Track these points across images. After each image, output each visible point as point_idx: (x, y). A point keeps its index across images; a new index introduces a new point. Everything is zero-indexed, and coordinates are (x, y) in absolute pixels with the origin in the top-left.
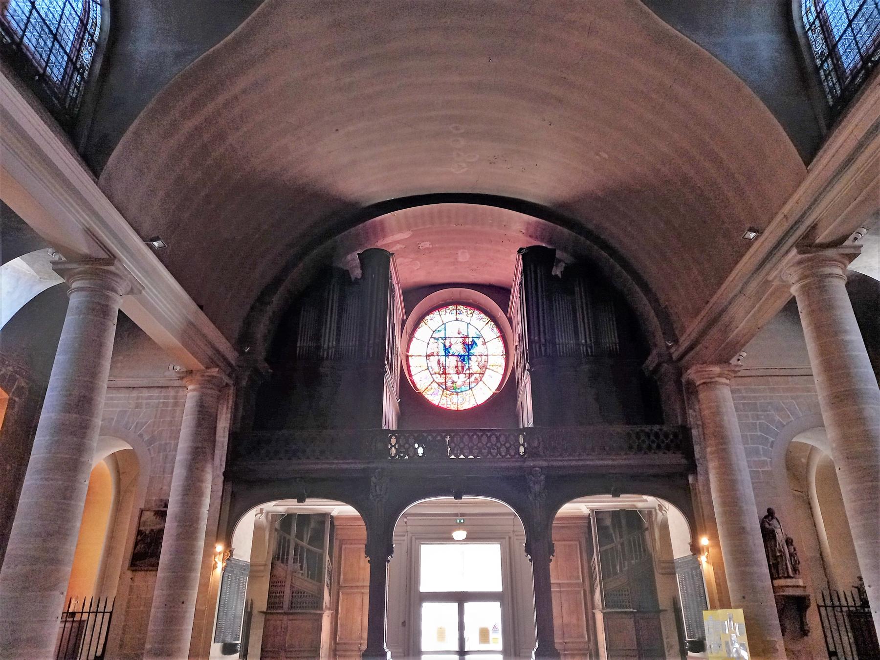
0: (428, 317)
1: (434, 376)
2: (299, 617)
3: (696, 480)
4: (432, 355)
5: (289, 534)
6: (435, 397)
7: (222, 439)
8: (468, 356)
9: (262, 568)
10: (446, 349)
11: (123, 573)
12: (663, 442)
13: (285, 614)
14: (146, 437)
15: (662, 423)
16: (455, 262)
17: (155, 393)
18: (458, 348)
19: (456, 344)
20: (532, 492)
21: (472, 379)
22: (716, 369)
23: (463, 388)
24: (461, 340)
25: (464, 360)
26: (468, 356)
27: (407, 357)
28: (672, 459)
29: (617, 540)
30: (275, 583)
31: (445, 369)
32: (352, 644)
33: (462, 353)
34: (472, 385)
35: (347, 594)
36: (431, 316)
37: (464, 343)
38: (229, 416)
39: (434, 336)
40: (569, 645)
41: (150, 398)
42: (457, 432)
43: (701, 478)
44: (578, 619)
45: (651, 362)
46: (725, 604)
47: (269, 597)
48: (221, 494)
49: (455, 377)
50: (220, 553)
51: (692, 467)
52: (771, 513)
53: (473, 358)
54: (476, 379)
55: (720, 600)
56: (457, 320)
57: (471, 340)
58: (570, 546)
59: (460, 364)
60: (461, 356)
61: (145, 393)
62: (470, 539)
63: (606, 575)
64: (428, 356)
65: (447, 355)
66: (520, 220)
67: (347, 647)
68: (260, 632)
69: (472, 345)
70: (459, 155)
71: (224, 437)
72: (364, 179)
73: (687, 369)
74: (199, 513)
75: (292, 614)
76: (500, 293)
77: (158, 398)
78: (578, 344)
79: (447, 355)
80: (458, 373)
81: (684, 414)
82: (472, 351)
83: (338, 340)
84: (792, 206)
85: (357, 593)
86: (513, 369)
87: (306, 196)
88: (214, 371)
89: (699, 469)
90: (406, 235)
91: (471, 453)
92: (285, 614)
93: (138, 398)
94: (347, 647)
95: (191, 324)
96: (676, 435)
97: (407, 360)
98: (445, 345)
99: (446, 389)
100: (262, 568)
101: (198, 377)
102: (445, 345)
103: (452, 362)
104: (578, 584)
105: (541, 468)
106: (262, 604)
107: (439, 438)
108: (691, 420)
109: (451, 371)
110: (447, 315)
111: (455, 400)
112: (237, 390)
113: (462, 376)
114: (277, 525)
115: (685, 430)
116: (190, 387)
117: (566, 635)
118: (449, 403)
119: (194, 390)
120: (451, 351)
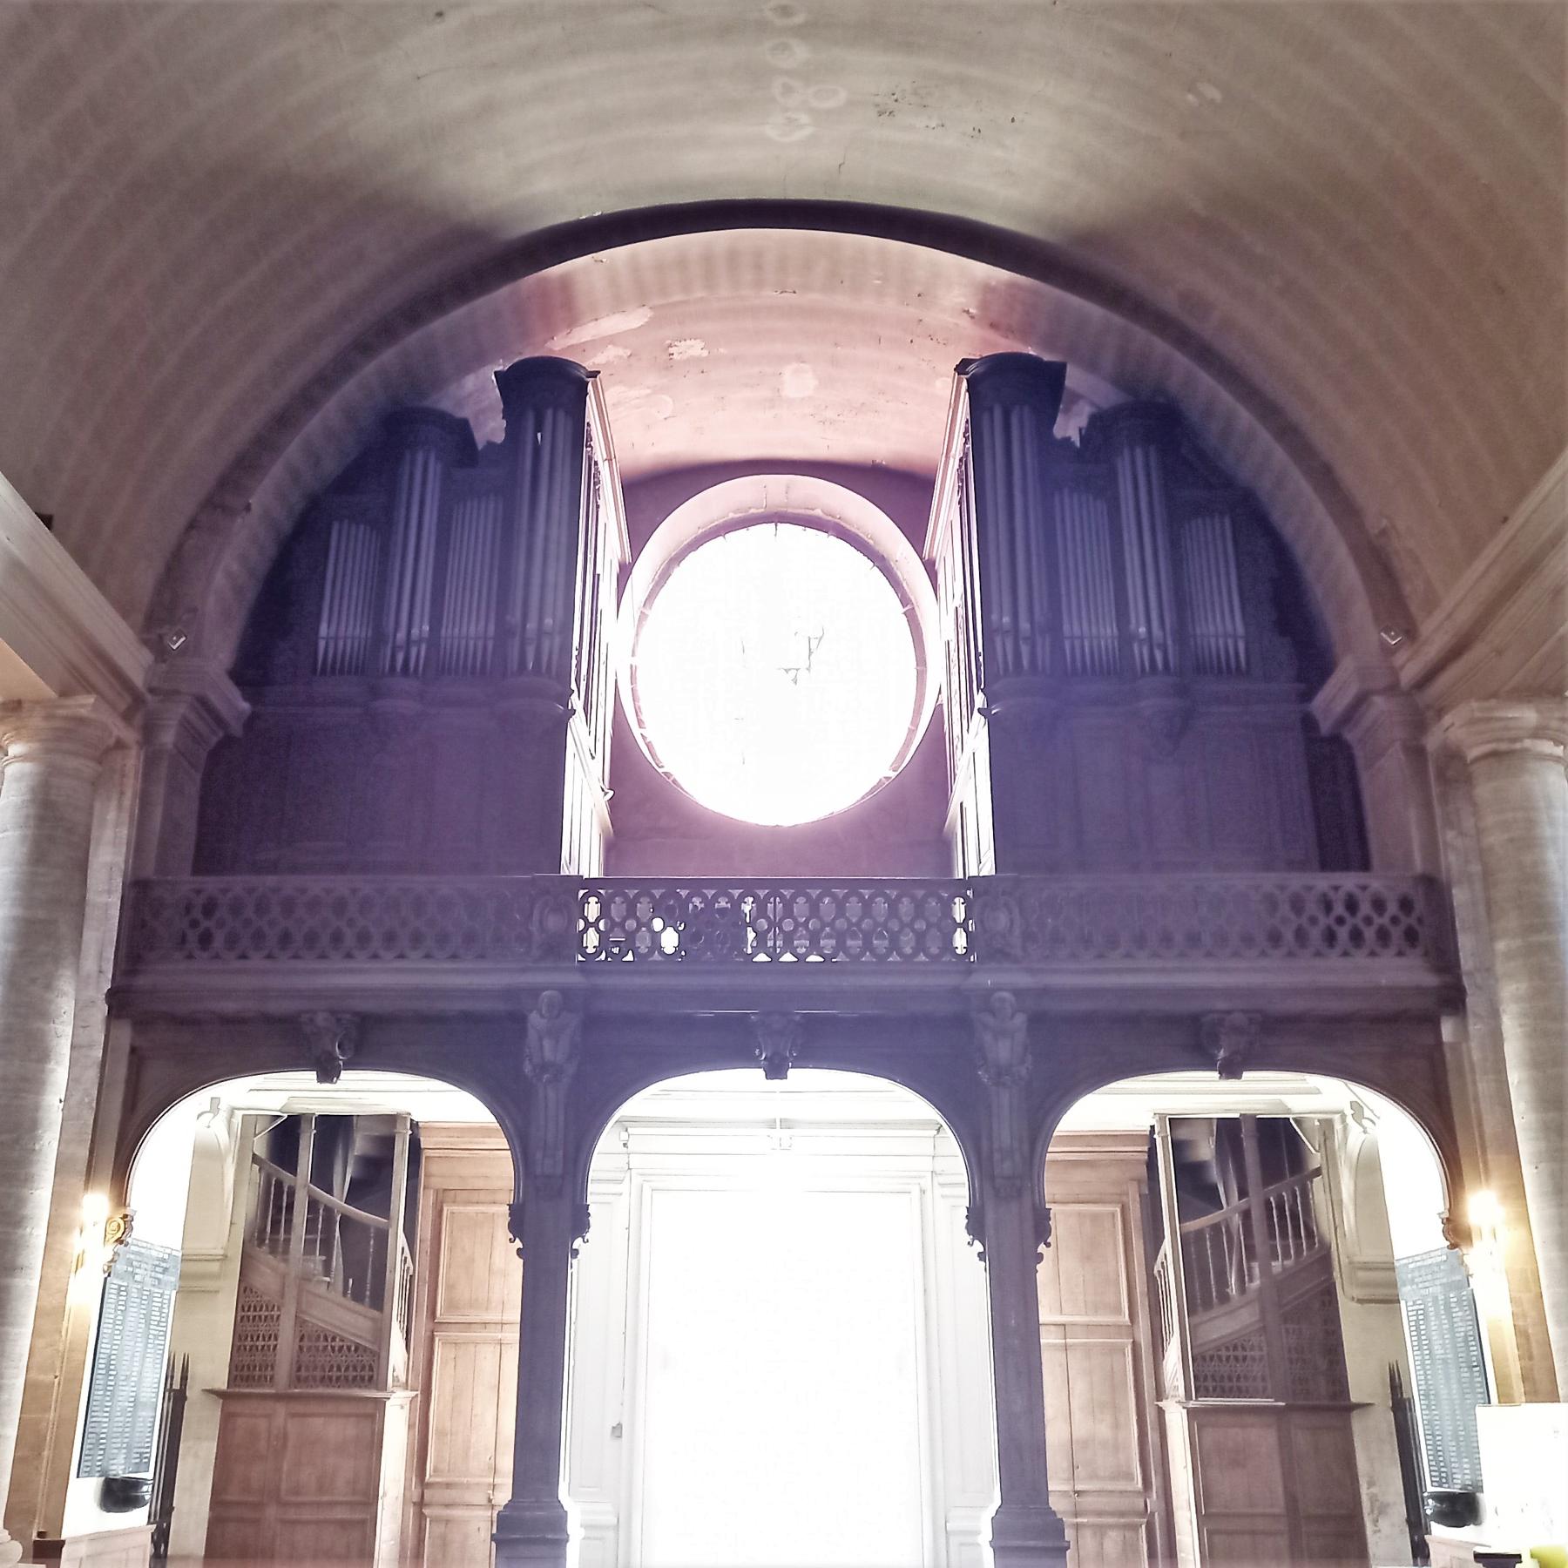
2: (313, 1407)
3: (1463, 1032)
7: (104, 899)
13: (278, 1397)
22: (1528, 715)
38: (125, 832)
43: (1475, 1028)
44: (1116, 1426)
45: (1333, 698)
47: (236, 1349)
48: (98, 1053)
51: (1453, 999)
66: (961, 278)
67: (453, 1494)
68: (209, 1449)
70: (788, 90)
71: (109, 892)
73: (1440, 713)
74: (37, 1108)
78: (1125, 638)
81: (1432, 847)
83: (436, 621)
86: (938, 710)
88: (84, 704)
90: (635, 319)
91: (789, 946)
92: (278, 1397)
94: (453, 1494)
96: (1406, 905)
100: (214, 1267)
101: (36, 721)
105: (566, 992)
106: (213, 1369)
114: (260, 1146)
115: (1434, 887)
116: (15, 749)
117: (1080, 1472)
119: (22, 758)
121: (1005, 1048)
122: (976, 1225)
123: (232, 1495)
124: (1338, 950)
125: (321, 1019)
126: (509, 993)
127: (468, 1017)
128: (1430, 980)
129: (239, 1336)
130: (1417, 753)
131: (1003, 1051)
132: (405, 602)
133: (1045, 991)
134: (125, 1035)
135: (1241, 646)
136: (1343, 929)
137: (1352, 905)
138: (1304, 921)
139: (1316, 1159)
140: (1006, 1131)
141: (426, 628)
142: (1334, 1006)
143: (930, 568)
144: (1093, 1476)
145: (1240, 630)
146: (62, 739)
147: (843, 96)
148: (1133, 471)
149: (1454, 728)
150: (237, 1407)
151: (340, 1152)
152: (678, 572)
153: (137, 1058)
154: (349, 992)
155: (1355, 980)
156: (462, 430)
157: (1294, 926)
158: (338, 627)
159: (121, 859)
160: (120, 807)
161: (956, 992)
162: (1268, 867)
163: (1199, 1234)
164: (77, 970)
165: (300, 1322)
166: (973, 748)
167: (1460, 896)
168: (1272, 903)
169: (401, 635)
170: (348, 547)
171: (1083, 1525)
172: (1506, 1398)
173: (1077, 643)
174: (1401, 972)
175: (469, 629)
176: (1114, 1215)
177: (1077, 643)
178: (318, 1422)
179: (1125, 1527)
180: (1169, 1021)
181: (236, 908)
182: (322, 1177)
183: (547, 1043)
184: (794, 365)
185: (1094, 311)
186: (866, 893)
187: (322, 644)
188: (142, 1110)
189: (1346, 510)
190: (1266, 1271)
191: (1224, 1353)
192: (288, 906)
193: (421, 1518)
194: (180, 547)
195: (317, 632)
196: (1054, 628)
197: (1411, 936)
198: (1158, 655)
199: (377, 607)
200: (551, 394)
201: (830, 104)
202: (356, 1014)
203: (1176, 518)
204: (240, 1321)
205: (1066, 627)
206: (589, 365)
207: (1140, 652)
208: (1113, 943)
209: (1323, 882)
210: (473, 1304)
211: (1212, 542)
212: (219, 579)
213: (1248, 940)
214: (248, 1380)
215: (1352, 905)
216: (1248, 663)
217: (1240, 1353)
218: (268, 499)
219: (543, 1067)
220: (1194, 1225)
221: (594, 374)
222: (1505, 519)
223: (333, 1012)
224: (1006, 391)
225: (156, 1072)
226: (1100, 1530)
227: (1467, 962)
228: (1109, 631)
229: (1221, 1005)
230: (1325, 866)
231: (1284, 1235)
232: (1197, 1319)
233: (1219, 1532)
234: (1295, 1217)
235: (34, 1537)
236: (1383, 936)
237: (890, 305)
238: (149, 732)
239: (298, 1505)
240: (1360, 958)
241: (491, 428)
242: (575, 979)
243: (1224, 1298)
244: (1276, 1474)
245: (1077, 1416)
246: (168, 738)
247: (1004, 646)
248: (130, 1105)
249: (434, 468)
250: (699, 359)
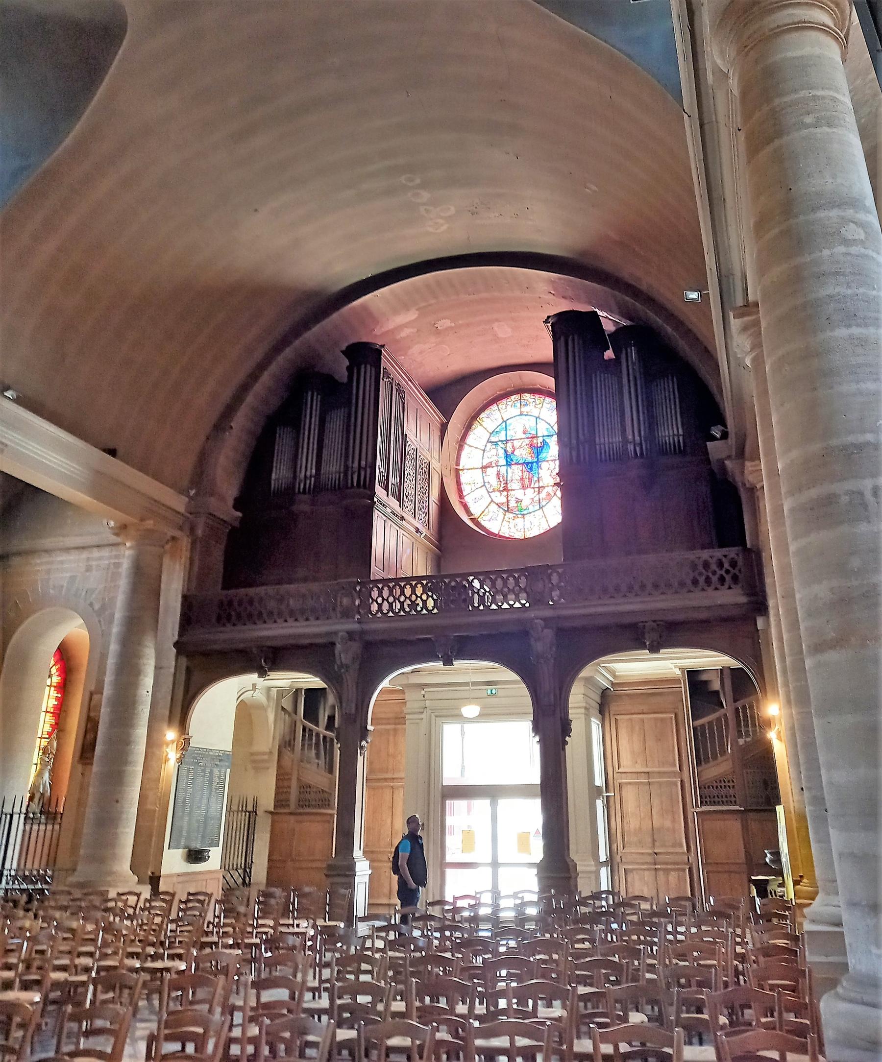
0: (483, 415)
1: (492, 495)
2: (305, 817)
4: (490, 465)
6: (496, 524)
8: (537, 462)
9: (266, 757)
10: (507, 456)
11: (73, 767)
12: (727, 572)
13: (291, 814)
14: (97, 607)
16: (497, 339)
17: (106, 552)
18: (523, 453)
19: (520, 447)
21: (543, 495)
23: (531, 509)
24: (527, 441)
25: (531, 469)
26: (537, 462)
27: (457, 471)
30: (282, 778)
31: (506, 483)
32: (380, 852)
33: (529, 459)
34: (543, 503)
36: (487, 412)
37: (531, 445)
39: (493, 439)
40: (660, 858)
41: (100, 558)
42: (487, 574)
44: (674, 821)
48: (173, 670)
49: (519, 494)
50: (173, 742)
53: (544, 465)
54: (548, 494)
55: (373, 904)
56: (521, 414)
57: (540, 440)
58: (662, 720)
59: (526, 475)
60: (527, 464)
61: (96, 553)
62: (485, 716)
64: (484, 468)
65: (509, 464)
69: (542, 447)
72: (325, 256)
74: (135, 696)
75: (300, 814)
77: (110, 557)
78: (625, 441)
79: (509, 464)
80: (523, 487)
82: (542, 456)
83: (318, 468)
85: (386, 787)
87: (245, 295)
88: (150, 524)
90: (412, 315)
91: (505, 599)
92: (291, 814)
93: (88, 559)
95: (98, 473)
97: (458, 477)
98: (506, 451)
99: (508, 510)
102: (506, 451)
103: (516, 472)
104: (674, 772)
105: (545, 619)
106: (268, 801)
107: (453, 584)
109: (515, 485)
110: (509, 408)
111: (520, 526)
112: (193, 543)
113: (529, 491)
114: (287, 704)
116: (128, 544)
117: (657, 844)
118: (513, 530)
119: (130, 548)
120: (514, 459)
121: (543, 643)
123: (274, 858)
124: (713, 587)
125: (255, 651)
129: (278, 787)
135: (681, 438)
136: (704, 577)
138: (696, 573)
140: (547, 685)
141: (314, 471)
142: (703, 615)
144: (663, 846)
145: (681, 432)
146: (146, 538)
147: (453, 210)
150: (276, 817)
151: (322, 703)
153: (189, 671)
154: (268, 638)
155: (707, 603)
157: (691, 577)
159: (181, 588)
160: (180, 564)
162: (692, 548)
163: (703, 726)
164: (156, 637)
168: (706, 565)
169: (356, 465)
171: (659, 869)
173: (602, 446)
174: (732, 597)
176: (671, 718)
177: (602, 446)
179: (678, 869)
181: (240, 603)
183: (344, 654)
184: (497, 324)
186: (505, 576)
187: (598, 447)
188: (191, 693)
190: (735, 743)
191: (715, 784)
192: (251, 602)
194: (204, 448)
195: (271, 475)
196: (592, 442)
197: (735, 579)
198: (638, 449)
200: (366, 356)
201: (448, 214)
202: (269, 647)
204: (277, 780)
205: (597, 439)
206: (380, 342)
209: (718, 553)
211: (667, 393)
212: (222, 460)
213: (682, 584)
214: (282, 806)
215: (706, 565)
216: (684, 446)
217: (723, 784)
218: (242, 421)
219: (342, 666)
220: (699, 722)
221: (383, 346)
223: (258, 647)
224: (567, 326)
225: (196, 677)
226: (667, 871)
228: (617, 439)
230: (721, 546)
231: (746, 726)
232: (700, 769)
233: (711, 872)
234: (745, 716)
235: (150, 873)
237: (517, 293)
238: (192, 529)
239: (313, 861)
240: (710, 591)
242: (548, 613)
243: (723, 752)
245: (655, 817)
246: (200, 532)
248: (186, 691)
250: (451, 328)
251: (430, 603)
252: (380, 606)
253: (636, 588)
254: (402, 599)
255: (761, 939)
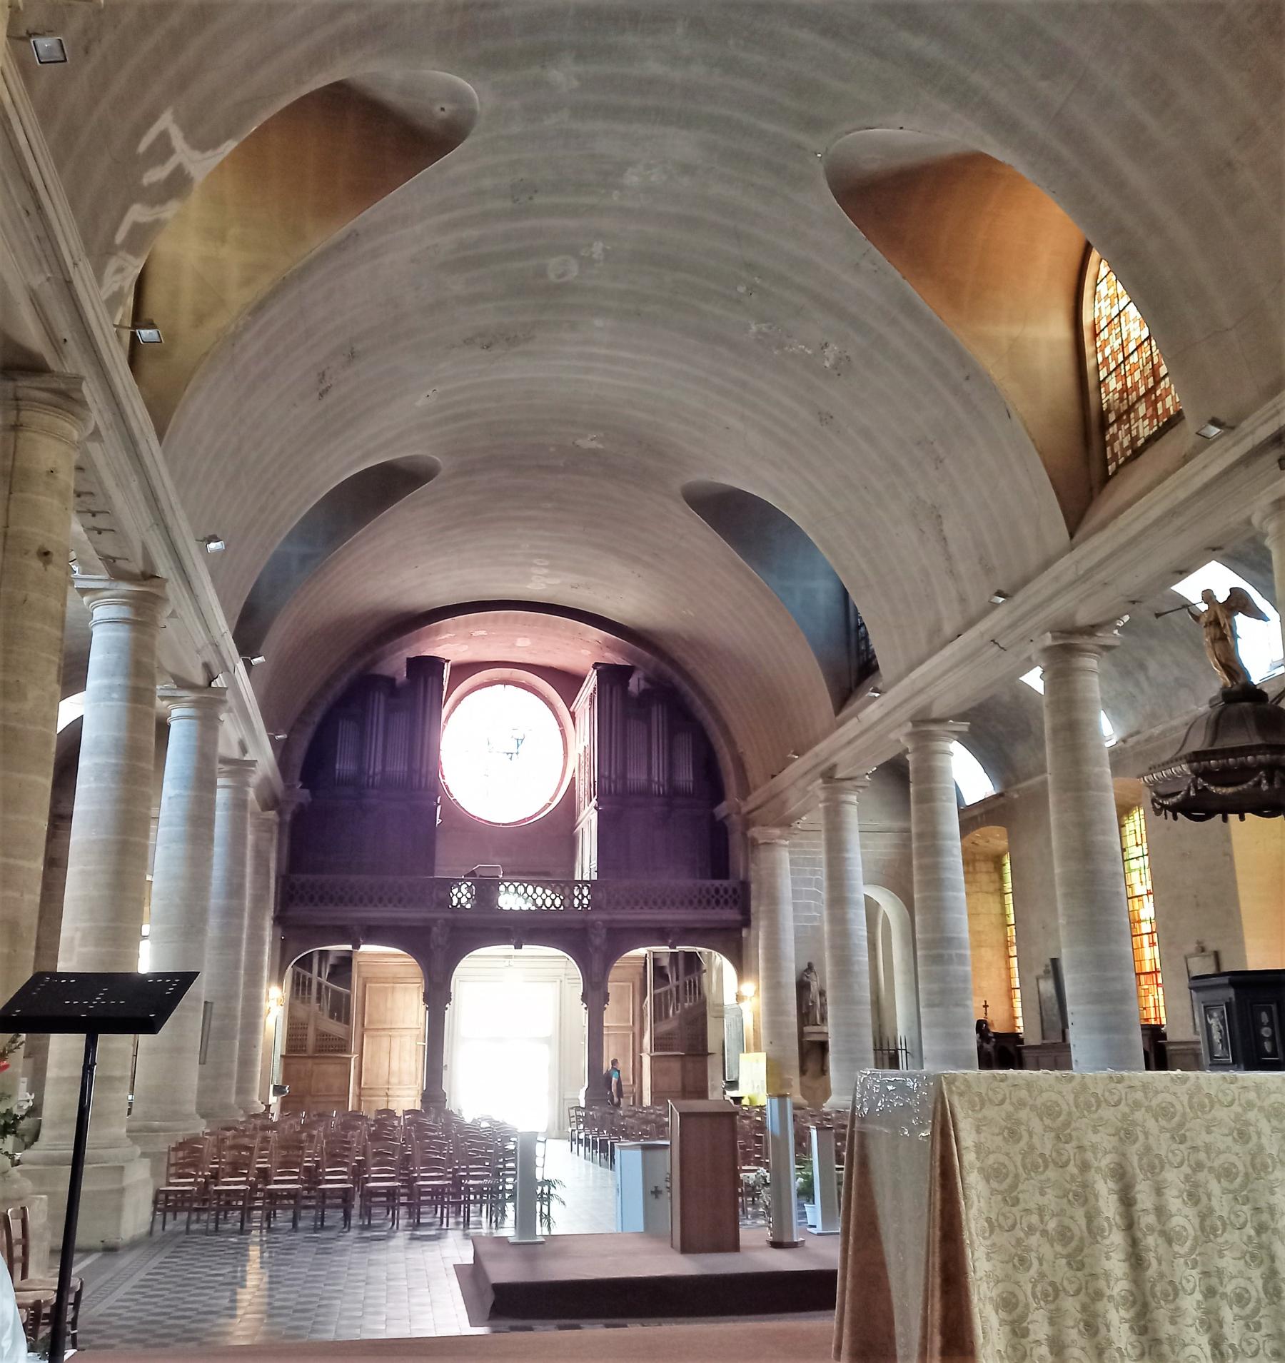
3: (749, 933)
5: (311, 971)
15: (726, 877)
16: (513, 645)
20: (587, 939)
22: (777, 831)
28: (730, 915)
29: (673, 981)
35: (373, 1037)
43: (753, 932)
45: (722, 810)
46: (757, 1049)
51: (747, 923)
52: (810, 967)
55: (755, 1044)
63: (659, 1014)
67: (371, 1092)
73: (754, 825)
76: (567, 682)
78: (650, 780)
81: (747, 870)
84: (822, 748)
86: (573, 779)
89: (753, 923)
94: (371, 1092)
96: (735, 891)
105: (446, 920)
108: (752, 874)
115: (745, 885)
121: (598, 940)
122: (585, 998)
126: (425, 920)
127: (410, 928)
128: (739, 917)
130: (744, 834)
131: (597, 941)
132: (367, 756)
133: (613, 921)
134: (279, 931)
136: (716, 899)
137: (717, 891)
139: (705, 966)
143: (573, 715)
148: (657, 715)
149: (755, 832)
150: (290, 1061)
152: (459, 707)
155: (716, 917)
156: (391, 680)
158: (344, 766)
161: (583, 921)
165: (316, 1029)
166: (588, 819)
167: (753, 887)
170: (347, 730)
172: (748, 1051)
175: (398, 767)
178: (324, 1067)
180: (652, 929)
182: (320, 975)
185: (647, 655)
189: (731, 743)
193: (360, 1100)
196: (624, 777)
197: (735, 902)
199: (360, 757)
203: (672, 733)
207: (655, 787)
208: (637, 903)
210: (385, 1022)
211: (685, 744)
215: (717, 891)
222: (773, 776)
227: (753, 910)
228: (644, 777)
229: (670, 925)
236: (726, 902)
240: (718, 910)
241: (403, 676)
242: (449, 916)
243: (667, 1015)
244: (679, 1079)
247: (605, 783)
249: (382, 697)
251: (558, 902)
252: (459, 899)
253: (668, 902)
254: (460, 895)
255: (306, 1229)
